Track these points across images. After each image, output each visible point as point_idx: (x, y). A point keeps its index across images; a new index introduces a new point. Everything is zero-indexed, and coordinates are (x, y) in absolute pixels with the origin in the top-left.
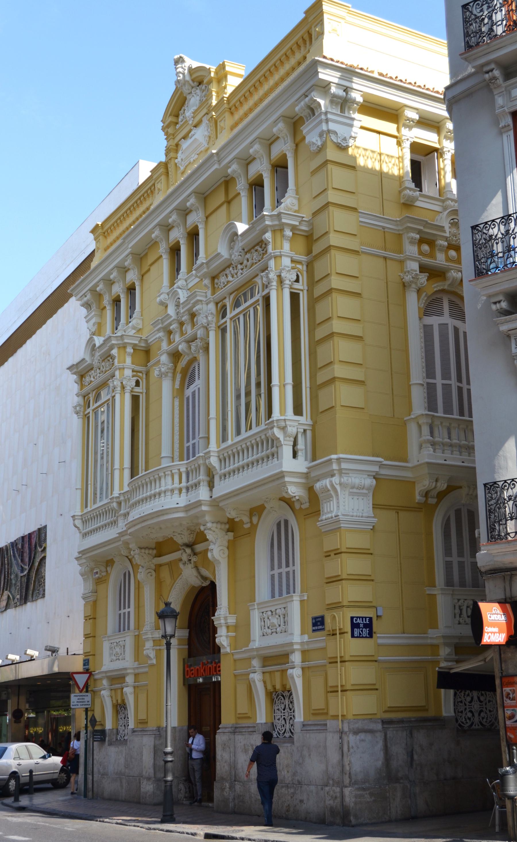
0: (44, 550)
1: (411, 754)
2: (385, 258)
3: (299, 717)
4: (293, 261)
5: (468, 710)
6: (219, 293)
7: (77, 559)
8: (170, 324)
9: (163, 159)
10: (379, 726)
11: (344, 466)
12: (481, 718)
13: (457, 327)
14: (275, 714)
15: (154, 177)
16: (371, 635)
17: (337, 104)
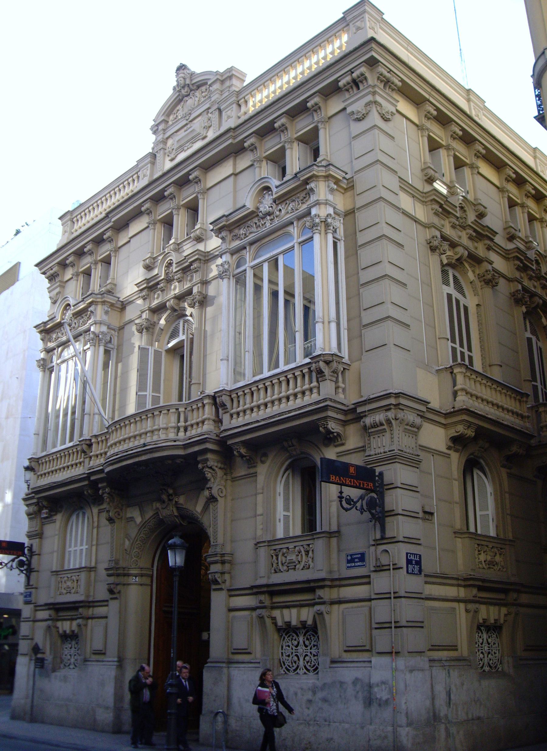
1: (449, 694)
5: (294, 654)
7: (25, 500)
10: (427, 665)
11: (403, 401)
12: (306, 663)
13: (459, 299)
14: (498, 648)
15: (139, 166)
17: (381, 81)
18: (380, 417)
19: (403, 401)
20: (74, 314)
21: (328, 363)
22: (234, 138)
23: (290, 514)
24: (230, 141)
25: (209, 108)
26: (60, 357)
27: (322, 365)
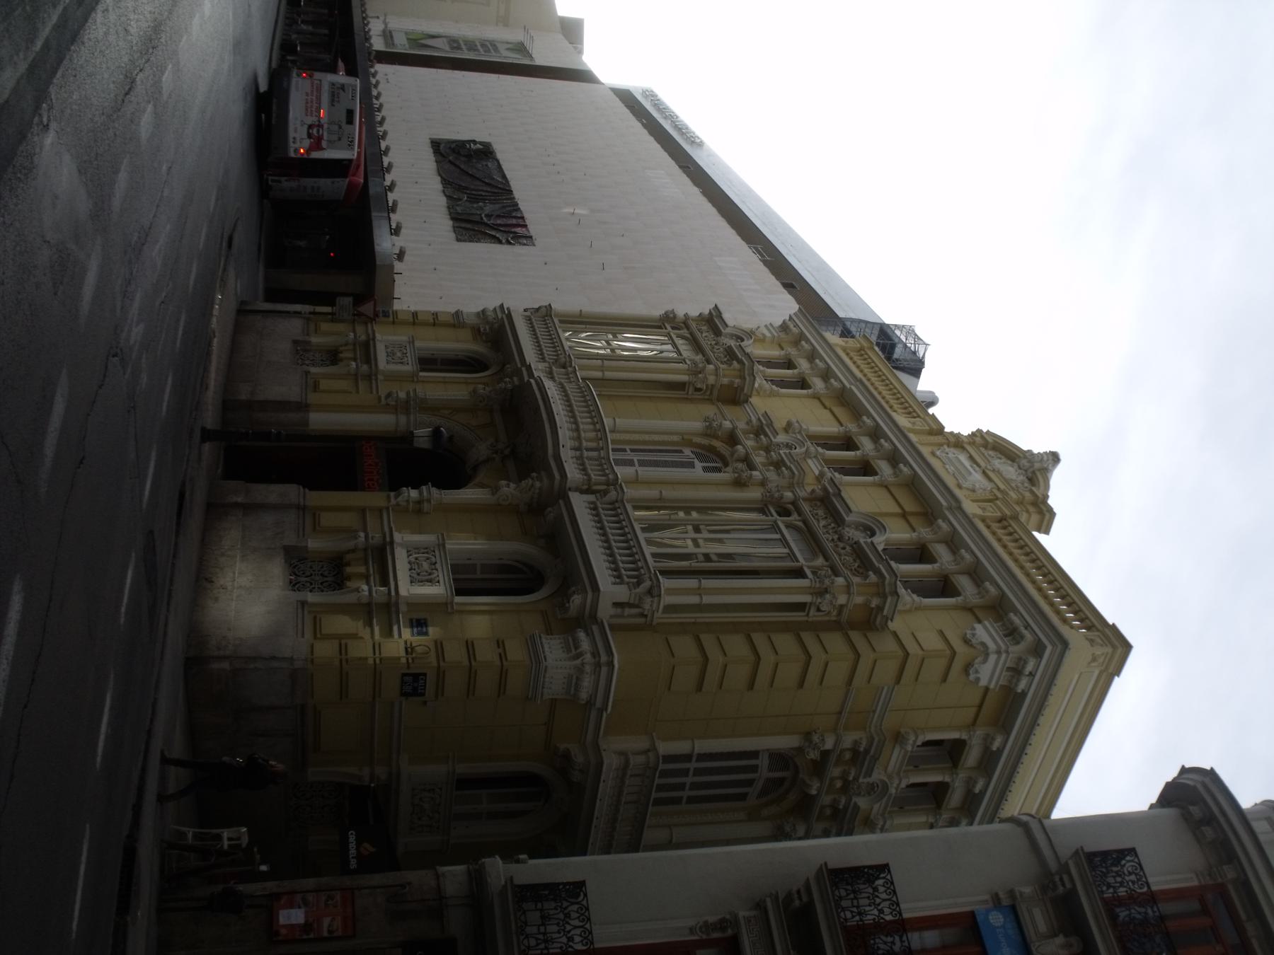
0: (509, 243)
2: (840, 713)
3: (313, 370)
4: (842, 606)
6: (806, 507)
7: (502, 306)
8: (766, 435)
9: (947, 430)
11: (604, 670)
16: (404, 694)
18: (585, 645)
19: (604, 670)
20: (730, 347)
21: (650, 592)
22: (950, 509)
23: (479, 575)
24: (944, 503)
25: (999, 489)
26: (683, 337)
27: (647, 584)
